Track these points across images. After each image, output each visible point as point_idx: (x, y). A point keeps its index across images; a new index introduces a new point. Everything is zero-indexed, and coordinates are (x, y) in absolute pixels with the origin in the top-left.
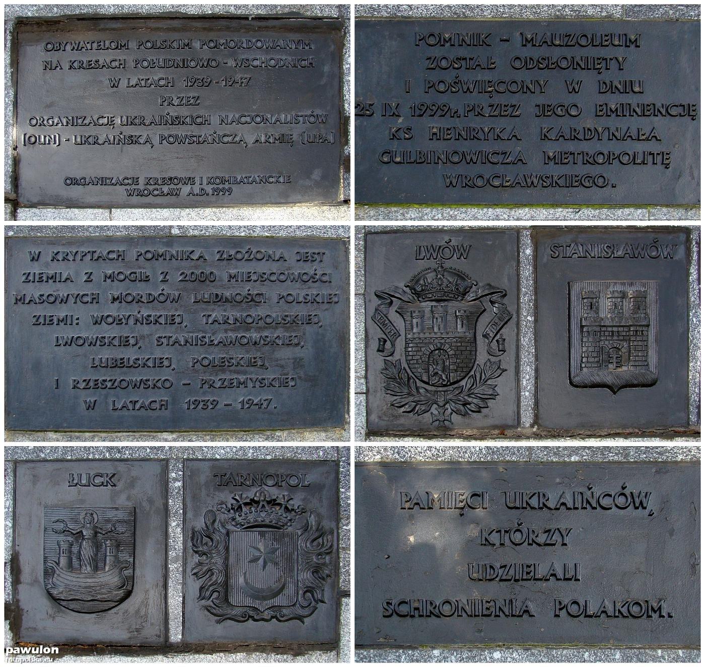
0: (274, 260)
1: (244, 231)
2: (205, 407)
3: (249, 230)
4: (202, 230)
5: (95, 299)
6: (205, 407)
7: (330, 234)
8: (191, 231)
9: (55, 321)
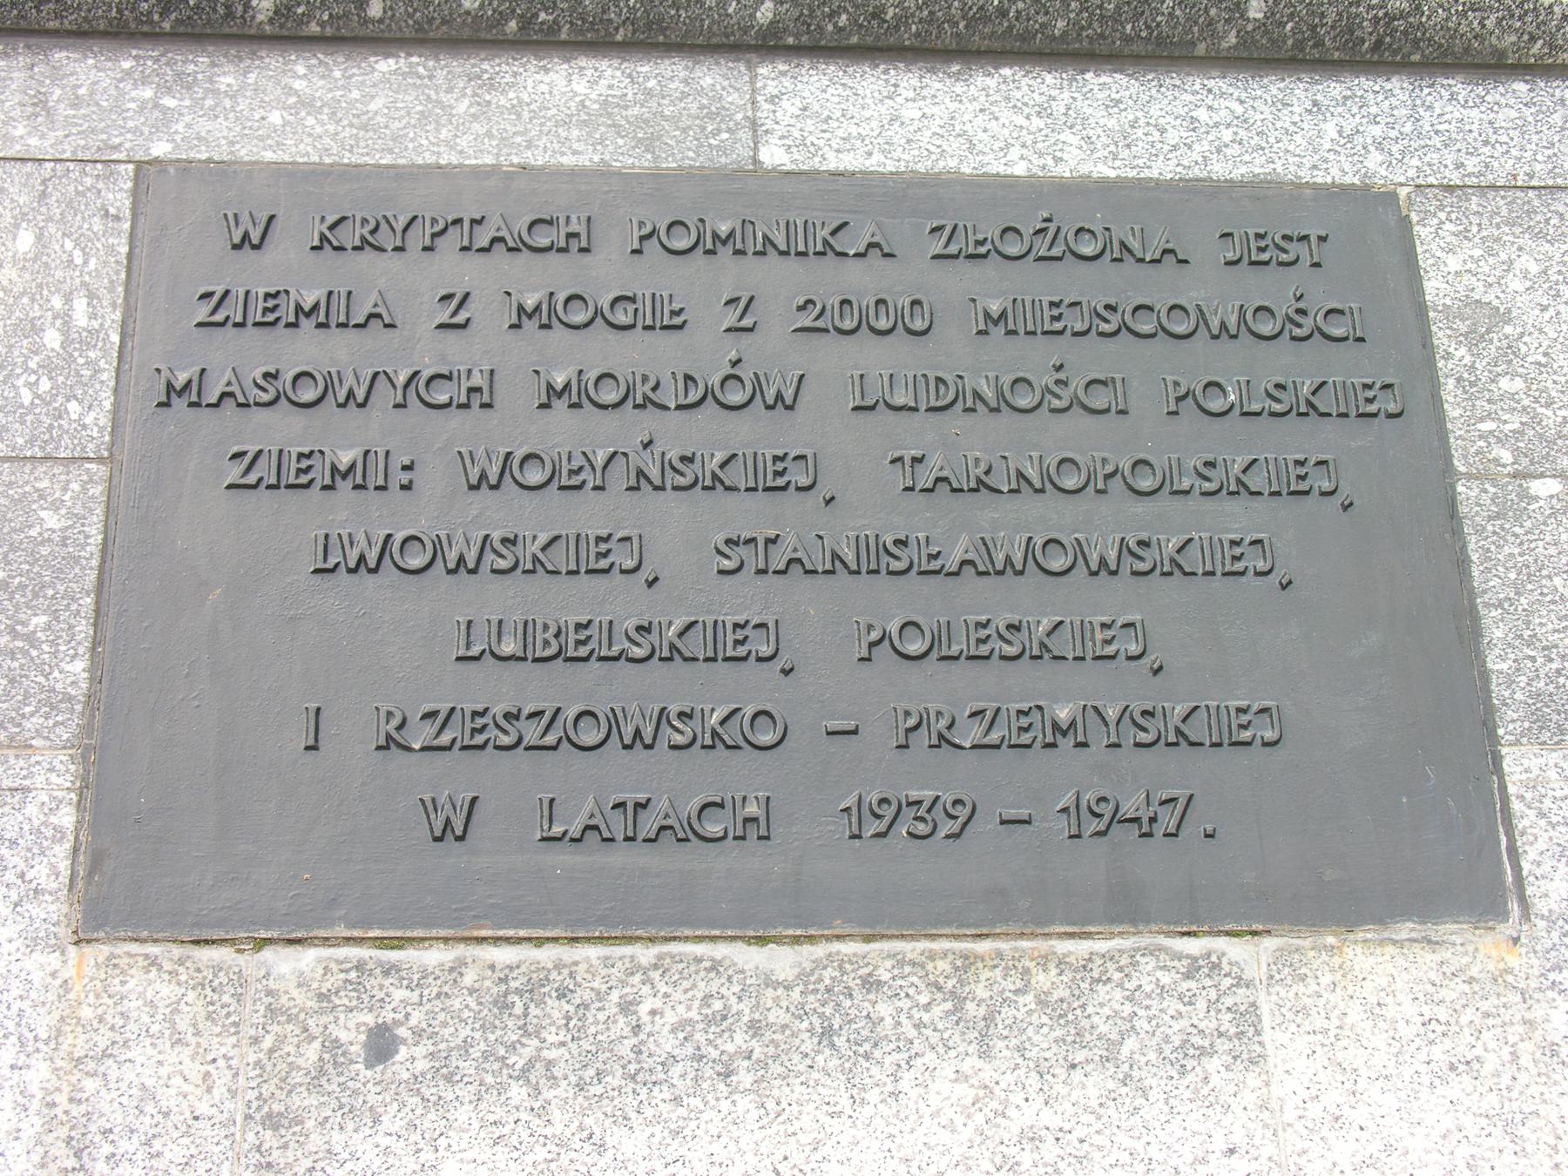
0: (1141, 260)
1: (1022, 158)
2: (922, 828)
3: (1041, 155)
4: (870, 154)
5: (480, 398)
6: (922, 828)
7: (1335, 171)
8: (831, 155)
9: (321, 475)
